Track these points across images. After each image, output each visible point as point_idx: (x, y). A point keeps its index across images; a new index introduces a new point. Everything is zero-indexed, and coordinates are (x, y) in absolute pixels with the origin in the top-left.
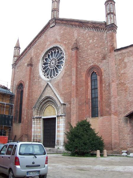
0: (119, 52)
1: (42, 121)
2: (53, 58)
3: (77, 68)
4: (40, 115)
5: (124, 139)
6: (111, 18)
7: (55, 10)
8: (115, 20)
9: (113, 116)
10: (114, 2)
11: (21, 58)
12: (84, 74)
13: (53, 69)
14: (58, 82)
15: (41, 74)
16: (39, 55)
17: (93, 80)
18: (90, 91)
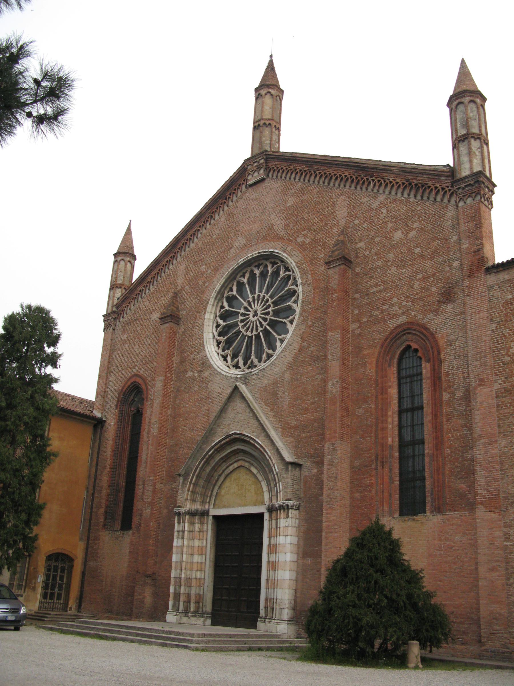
1: (209, 526)
4: (203, 503)
6: (470, 153)
7: (266, 124)
9: (483, 514)
13: (258, 337)
14: (275, 383)
17: (406, 377)
18: (396, 419)
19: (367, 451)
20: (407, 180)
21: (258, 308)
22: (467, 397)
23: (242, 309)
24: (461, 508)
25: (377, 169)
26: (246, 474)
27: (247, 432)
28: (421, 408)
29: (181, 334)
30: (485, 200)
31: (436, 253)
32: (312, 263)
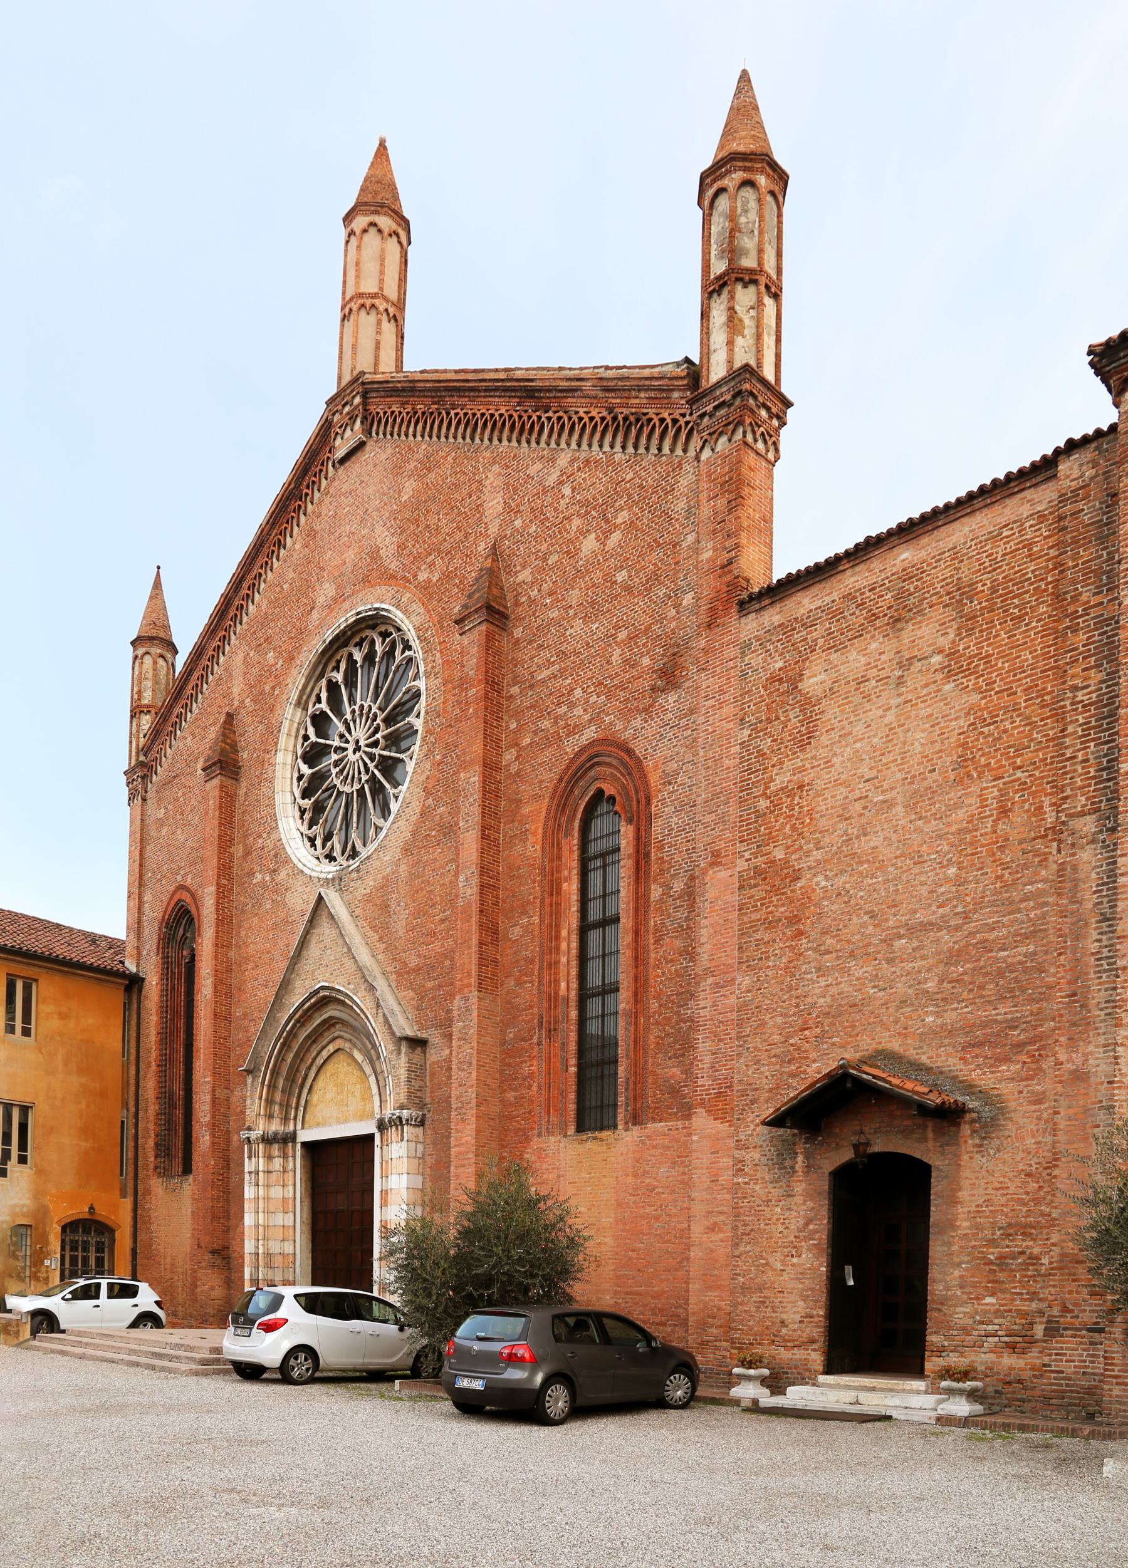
0: (773, 616)
1: (297, 1162)
2: (357, 708)
3: (490, 767)
4: (285, 1120)
5: (760, 1289)
6: (733, 323)
7: (377, 306)
8: (769, 341)
9: (702, 1121)
10: (774, 166)
11: (174, 719)
12: (535, 812)
13: (361, 792)
14: (386, 884)
15: (290, 829)
16: (273, 688)
17: (596, 858)
18: (574, 945)
19: (525, 1010)
20: (610, 410)
21: (360, 733)
22: (690, 895)
23: (337, 738)
24: (670, 1114)
25: (556, 389)
26: (348, 1064)
27: (339, 984)
28: (616, 920)
29: (242, 799)
30: (756, 440)
31: (654, 578)
32: (442, 627)
